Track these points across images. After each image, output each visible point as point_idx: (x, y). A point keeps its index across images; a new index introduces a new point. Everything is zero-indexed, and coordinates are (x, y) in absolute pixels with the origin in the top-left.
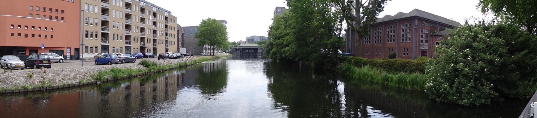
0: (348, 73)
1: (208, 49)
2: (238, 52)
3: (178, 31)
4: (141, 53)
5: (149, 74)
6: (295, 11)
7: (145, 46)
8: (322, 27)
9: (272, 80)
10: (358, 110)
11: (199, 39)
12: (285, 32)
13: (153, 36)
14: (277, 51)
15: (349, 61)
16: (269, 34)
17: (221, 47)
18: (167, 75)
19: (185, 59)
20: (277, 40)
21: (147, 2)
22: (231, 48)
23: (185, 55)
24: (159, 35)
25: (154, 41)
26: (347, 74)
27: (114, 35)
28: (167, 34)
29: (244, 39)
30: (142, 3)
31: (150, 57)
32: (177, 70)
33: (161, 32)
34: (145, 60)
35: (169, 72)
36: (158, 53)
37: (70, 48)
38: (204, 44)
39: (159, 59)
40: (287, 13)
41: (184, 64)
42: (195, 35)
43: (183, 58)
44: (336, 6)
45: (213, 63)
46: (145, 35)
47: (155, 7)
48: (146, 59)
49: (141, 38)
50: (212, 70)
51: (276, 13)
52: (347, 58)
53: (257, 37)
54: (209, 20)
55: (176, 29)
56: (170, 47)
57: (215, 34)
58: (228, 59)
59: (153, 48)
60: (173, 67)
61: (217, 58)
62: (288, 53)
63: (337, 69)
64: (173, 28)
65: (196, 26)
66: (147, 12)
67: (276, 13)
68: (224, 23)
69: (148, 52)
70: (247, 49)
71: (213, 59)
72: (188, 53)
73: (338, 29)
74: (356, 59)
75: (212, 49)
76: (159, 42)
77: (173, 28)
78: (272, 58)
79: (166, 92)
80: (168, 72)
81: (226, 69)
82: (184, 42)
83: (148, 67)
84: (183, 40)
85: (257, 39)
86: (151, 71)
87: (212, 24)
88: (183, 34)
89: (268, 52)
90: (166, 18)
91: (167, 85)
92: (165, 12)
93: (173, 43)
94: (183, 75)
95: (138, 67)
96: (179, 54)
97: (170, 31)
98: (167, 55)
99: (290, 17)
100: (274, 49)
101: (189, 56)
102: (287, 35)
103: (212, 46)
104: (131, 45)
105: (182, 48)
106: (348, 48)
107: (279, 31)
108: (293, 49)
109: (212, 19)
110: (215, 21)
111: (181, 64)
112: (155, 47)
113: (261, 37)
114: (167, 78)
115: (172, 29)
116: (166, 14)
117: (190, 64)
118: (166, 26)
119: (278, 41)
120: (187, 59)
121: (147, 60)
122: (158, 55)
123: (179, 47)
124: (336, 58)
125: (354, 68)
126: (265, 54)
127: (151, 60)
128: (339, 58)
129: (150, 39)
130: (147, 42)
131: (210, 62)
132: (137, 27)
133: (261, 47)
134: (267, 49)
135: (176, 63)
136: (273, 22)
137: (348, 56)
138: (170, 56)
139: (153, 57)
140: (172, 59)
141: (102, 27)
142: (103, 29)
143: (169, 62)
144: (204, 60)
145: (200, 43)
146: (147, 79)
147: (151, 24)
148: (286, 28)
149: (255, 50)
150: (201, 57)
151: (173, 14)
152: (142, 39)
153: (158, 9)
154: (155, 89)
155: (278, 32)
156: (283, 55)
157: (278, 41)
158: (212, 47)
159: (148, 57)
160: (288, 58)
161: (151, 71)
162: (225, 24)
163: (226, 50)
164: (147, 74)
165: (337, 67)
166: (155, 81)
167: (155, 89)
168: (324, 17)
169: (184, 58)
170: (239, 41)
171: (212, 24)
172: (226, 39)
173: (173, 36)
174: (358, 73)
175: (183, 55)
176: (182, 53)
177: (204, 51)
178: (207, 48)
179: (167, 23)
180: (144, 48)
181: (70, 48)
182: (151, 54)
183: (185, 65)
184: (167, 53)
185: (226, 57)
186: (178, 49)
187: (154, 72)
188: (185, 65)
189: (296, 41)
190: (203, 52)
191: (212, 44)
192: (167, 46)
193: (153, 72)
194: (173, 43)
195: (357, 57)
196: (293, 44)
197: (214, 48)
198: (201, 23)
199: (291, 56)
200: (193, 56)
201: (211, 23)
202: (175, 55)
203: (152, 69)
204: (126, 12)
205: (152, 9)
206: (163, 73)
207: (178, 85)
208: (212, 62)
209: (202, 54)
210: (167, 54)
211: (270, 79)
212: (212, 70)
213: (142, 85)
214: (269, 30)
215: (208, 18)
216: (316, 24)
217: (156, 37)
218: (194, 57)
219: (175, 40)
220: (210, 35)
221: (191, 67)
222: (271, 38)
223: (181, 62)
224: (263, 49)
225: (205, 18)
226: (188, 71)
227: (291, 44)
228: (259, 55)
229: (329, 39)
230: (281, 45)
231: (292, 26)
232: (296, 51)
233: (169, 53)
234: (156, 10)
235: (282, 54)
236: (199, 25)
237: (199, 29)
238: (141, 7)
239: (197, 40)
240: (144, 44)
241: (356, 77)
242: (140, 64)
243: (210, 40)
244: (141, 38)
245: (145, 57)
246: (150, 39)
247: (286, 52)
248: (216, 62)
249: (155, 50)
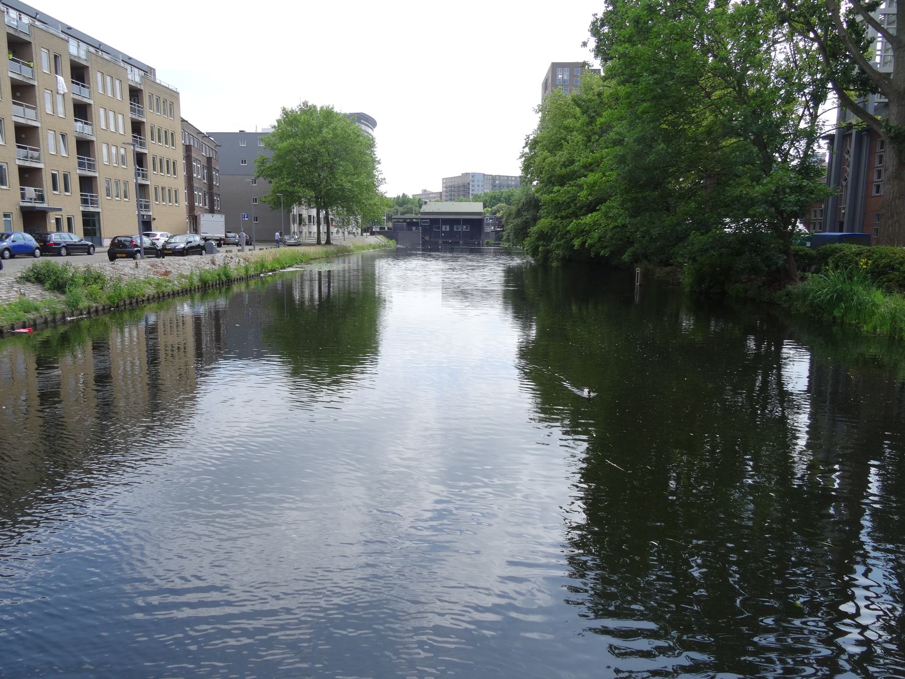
0: (837, 313)
1: (310, 221)
2: (417, 234)
3: (188, 149)
4: (28, 236)
5: (69, 319)
6: (627, 72)
7: (45, 205)
8: (730, 131)
9: (533, 333)
10: (872, 462)
11: (273, 184)
12: (583, 158)
14: (553, 229)
15: (846, 264)
16: (526, 168)
17: (353, 213)
18: (152, 319)
19: (221, 255)
20: (556, 188)
21: (37, 13)
22: (389, 218)
23: (220, 242)
24: (105, 159)
25: (87, 184)
26: (834, 318)
28: (140, 159)
29: (437, 187)
30: (13, 14)
31: (72, 249)
32: (192, 298)
33: (114, 150)
34: (48, 264)
35: (160, 308)
36: (108, 233)
38: (294, 201)
39: (113, 256)
40: (596, 81)
41: (219, 275)
43: (212, 253)
44: (797, 38)
45: (329, 271)
46: (38, 158)
47: (81, 38)
48: (53, 260)
49: (23, 171)
50: (324, 295)
51: (549, 89)
52: (834, 251)
53: (481, 178)
54: (308, 110)
55: (180, 142)
56: (156, 210)
57: (332, 168)
58: (381, 257)
59: (85, 214)
60: (176, 288)
61: (343, 253)
62: (596, 235)
63: (787, 295)
64: (167, 137)
65: (260, 131)
66: (43, 59)
67: (549, 89)
68: (363, 127)
69: (59, 228)
70: (446, 222)
71: (327, 257)
72: (233, 234)
73: (798, 135)
74: (875, 256)
75: (322, 221)
76: (108, 190)
77: (167, 137)
78: (534, 252)
79: (154, 386)
80: (154, 305)
81: (374, 290)
82: (215, 190)
83: (64, 293)
84: (210, 186)
85: (481, 184)
86: (81, 306)
87: (321, 127)
88: (209, 160)
89: (521, 233)
90: (135, 94)
91: (153, 359)
92: (129, 67)
93: (169, 195)
94: (217, 316)
95: (13, 294)
96: (197, 239)
97: (152, 149)
98: (147, 241)
99: (606, 100)
100: (544, 223)
101: (237, 244)
102: (589, 167)
103: (322, 208)
105: (210, 215)
106: (836, 210)
107: (562, 156)
108: (614, 219)
109: (319, 109)
110: (328, 114)
111: (209, 277)
112: (91, 209)
113: (494, 178)
114: (152, 330)
115: (163, 139)
116: (135, 77)
117: (243, 273)
118: (137, 127)
119: (561, 193)
120: (229, 255)
121: (58, 261)
122: (107, 243)
123: (197, 213)
124: (786, 252)
125: (869, 294)
126: (511, 237)
127: (79, 262)
128: (796, 254)
130: (55, 188)
131: (316, 268)
132: (63, 136)
133: (495, 213)
134: (518, 221)
135: (187, 273)
136: (543, 120)
137: (837, 245)
138: (160, 243)
139: (87, 250)
140: (167, 258)
143: (159, 270)
144: (294, 261)
145: (279, 198)
146: (65, 339)
147: (64, 111)
148: (590, 141)
149: (475, 224)
150: (283, 249)
151: (163, 77)
152: (28, 176)
153: (92, 50)
154: (103, 378)
155: (557, 158)
156: (577, 243)
157: (559, 191)
158: (323, 213)
159: (63, 251)
160: (592, 255)
161: (81, 306)
162: (370, 131)
163: (374, 223)
164: (64, 318)
165: (789, 287)
166: (100, 347)
167: (103, 378)
168: (741, 90)
169: (219, 255)
170: (419, 192)
171: (321, 127)
172: (371, 187)
173: (169, 167)
174: (888, 316)
175: (214, 243)
176: (208, 235)
177: (294, 227)
178: (305, 214)
179: (141, 113)
180: (42, 214)
182: (76, 237)
183: (223, 277)
184: (148, 235)
185: (374, 248)
186: (194, 223)
187: (92, 310)
188: (223, 277)
189: (627, 191)
190: (288, 231)
191: (324, 201)
192: (147, 207)
193: (89, 308)
194: (169, 195)
195: (884, 248)
196: (614, 203)
197: (330, 217)
198: (278, 121)
199: (606, 247)
200: (251, 247)
201: (314, 123)
202: (180, 242)
203: (84, 299)
205: (67, 49)
206: (132, 311)
207: (199, 354)
208: (325, 268)
209: (286, 237)
210: (145, 239)
211: (526, 327)
212: (324, 295)
213: (43, 364)
214: (527, 150)
215: (305, 104)
216: (709, 119)
217: (91, 167)
218: (257, 248)
219: (179, 182)
220: (312, 169)
221: (248, 286)
222: (531, 181)
223: (207, 267)
224: (504, 220)
225: (294, 105)
226: (237, 300)
227: (605, 201)
228: (487, 243)
229: (757, 180)
230: (569, 207)
231: (612, 135)
232: (624, 226)
233: (155, 235)
234: (83, 55)
235: (573, 239)
236: (272, 130)
237: (270, 146)
238: (11, 31)
239: (265, 188)
240: (41, 198)
241: (875, 329)
242: (26, 279)
243: (312, 186)
244: (23, 171)
245: (48, 249)
246: (66, 177)
247: (588, 232)
248: (336, 267)
249: (91, 223)
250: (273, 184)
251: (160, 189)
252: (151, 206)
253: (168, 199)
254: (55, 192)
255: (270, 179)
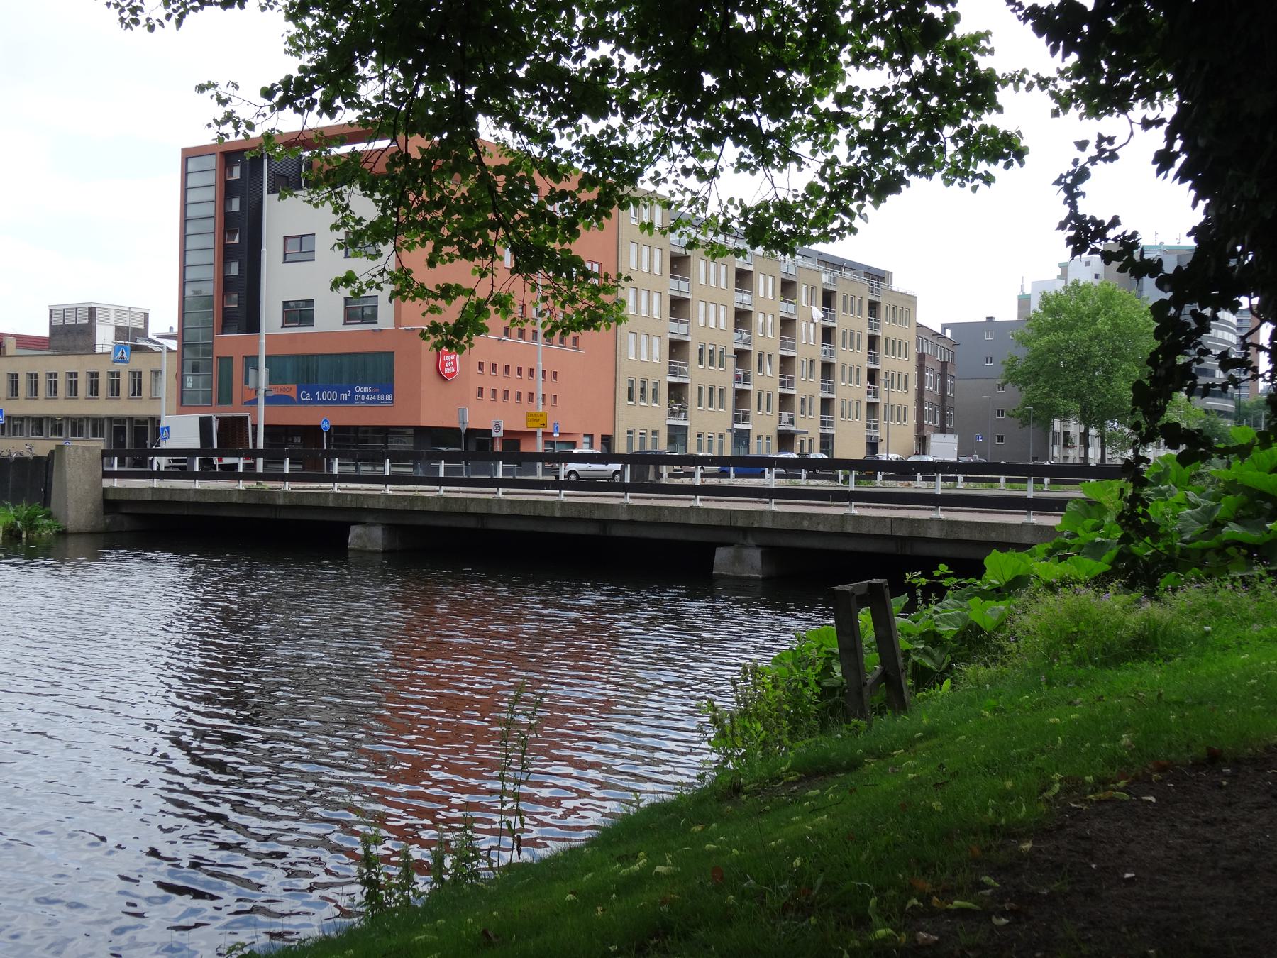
3: (921, 357)
7: (793, 429)
13: (823, 387)
27: (700, 389)
37: (591, 436)
42: (1002, 370)
55: (913, 351)
64: (900, 348)
66: (803, 293)
77: (900, 348)
82: (948, 403)
87: (1095, 314)
88: (944, 365)
97: (887, 363)
104: (749, 427)
105: (941, 435)
112: (828, 431)
123: (926, 432)
129: (769, 395)
130: (630, 399)
141: (670, 363)
142: (672, 372)
181: (591, 436)
186: (922, 443)
204: (737, 306)
219: (907, 398)
237: (1024, 341)
239: (1014, 396)
240: (792, 422)
243: (1079, 396)
250: (1024, 394)
251: (707, 391)
252: (879, 426)
253: (717, 403)
254: (630, 403)
255: (1021, 386)
